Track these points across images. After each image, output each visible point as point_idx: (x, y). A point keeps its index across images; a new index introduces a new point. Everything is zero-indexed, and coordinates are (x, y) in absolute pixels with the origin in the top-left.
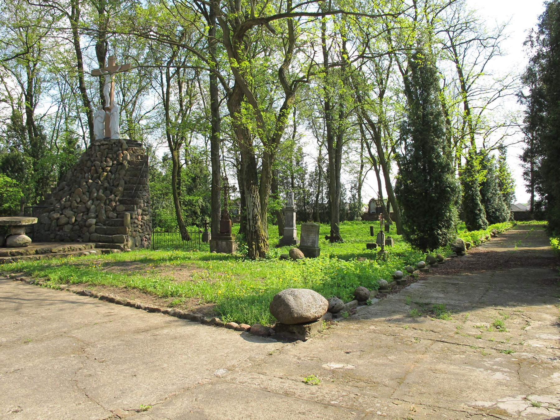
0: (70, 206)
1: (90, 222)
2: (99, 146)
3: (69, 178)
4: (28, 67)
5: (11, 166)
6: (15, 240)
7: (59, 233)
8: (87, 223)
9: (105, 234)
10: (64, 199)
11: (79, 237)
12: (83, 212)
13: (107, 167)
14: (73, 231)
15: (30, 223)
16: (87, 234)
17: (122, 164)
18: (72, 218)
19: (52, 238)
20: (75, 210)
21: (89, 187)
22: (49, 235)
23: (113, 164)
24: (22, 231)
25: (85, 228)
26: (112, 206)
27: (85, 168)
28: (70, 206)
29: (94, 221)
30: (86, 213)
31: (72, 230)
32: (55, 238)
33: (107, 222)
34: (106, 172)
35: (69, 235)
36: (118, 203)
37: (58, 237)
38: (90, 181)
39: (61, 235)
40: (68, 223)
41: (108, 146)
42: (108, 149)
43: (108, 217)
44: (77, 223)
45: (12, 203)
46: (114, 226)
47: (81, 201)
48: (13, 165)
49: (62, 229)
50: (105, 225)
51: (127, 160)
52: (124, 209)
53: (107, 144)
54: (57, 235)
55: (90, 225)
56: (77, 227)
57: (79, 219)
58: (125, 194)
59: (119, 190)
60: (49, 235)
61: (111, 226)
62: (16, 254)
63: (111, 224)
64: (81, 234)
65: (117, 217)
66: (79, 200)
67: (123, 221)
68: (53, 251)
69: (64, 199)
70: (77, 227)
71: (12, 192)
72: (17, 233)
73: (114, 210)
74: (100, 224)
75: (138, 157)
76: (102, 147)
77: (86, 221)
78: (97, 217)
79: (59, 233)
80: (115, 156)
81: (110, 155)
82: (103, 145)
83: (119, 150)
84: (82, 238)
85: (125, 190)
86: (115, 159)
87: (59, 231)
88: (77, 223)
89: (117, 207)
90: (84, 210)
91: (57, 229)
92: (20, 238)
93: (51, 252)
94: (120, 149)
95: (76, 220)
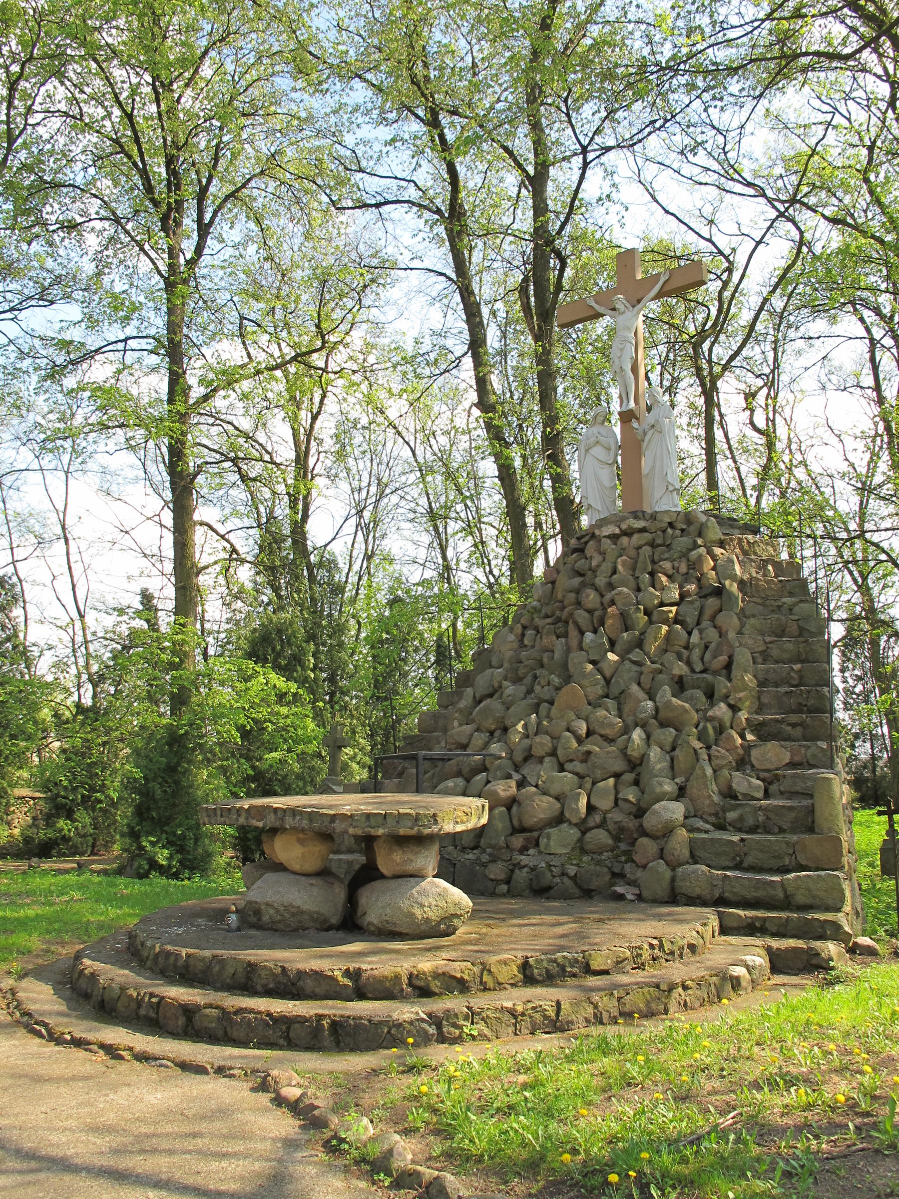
0: (553, 753)
1: (667, 816)
2: (614, 538)
3: (509, 654)
4: (294, 420)
5: (273, 649)
6: (404, 904)
7: (524, 859)
8: (650, 821)
9: (738, 867)
10: (520, 727)
11: (618, 876)
12: (617, 776)
13: (662, 604)
14: (583, 851)
15: (470, 826)
16: (661, 865)
17: (719, 592)
18: (577, 798)
19: (497, 882)
20: (578, 767)
21: (608, 681)
22: (484, 865)
23: (682, 596)
24: (429, 860)
25: (644, 841)
26: (731, 749)
27: (581, 616)
28: (553, 753)
29: (676, 810)
30: (629, 777)
31: (581, 848)
32: (508, 882)
33: (731, 816)
34: (665, 622)
35: (572, 870)
36: (750, 737)
37: (521, 876)
38: (612, 657)
39: (533, 869)
40: (559, 819)
41: (647, 536)
42: (653, 545)
43: (730, 794)
44: (597, 818)
45: (289, 750)
46: (768, 831)
47: (589, 733)
48: (279, 647)
49: (537, 844)
50: (721, 827)
51: (733, 577)
52: (787, 758)
53: (643, 530)
54: (519, 866)
55: (668, 831)
56: (600, 837)
57: (604, 803)
58: (765, 700)
59: (745, 687)
60: (484, 865)
61: (752, 830)
62: (435, 986)
63: (750, 821)
64: (628, 868)
65: (767, 795)
66: (582, 728)
67: (811, 811)
68: (595, 965)
69: (520, 727)
70: (600, 837)
71: (287, 717)
72: (410, 868)
73: (742, 763)
74: (700, 824)
75: (764, 567)
76: (625, 540)
77: (640, 812)
78: (681, 793)
79: (524, 859)
80: (683, 568)
81: (667, 565)
82: (628, 533)
83: (696, 546)
84: (633, 883)
85: (762, 684)
86: (686, 578)
87: (523, 850)
88: (597, 818)
89: (754, 753)
90: (619, 765)
91: (518, 841)
92: (424, 893)
93: (588, 970)
94: (700, 541)
95: (590, 808)
